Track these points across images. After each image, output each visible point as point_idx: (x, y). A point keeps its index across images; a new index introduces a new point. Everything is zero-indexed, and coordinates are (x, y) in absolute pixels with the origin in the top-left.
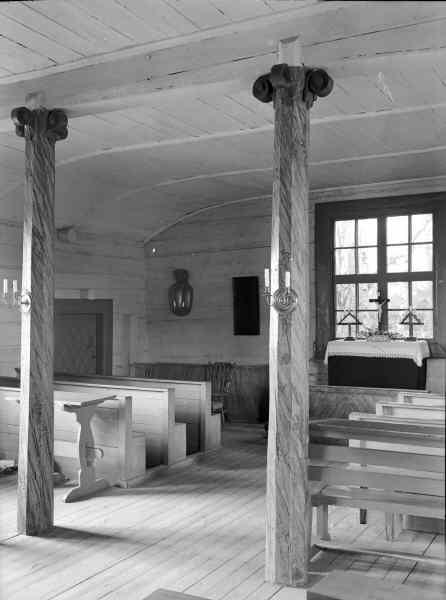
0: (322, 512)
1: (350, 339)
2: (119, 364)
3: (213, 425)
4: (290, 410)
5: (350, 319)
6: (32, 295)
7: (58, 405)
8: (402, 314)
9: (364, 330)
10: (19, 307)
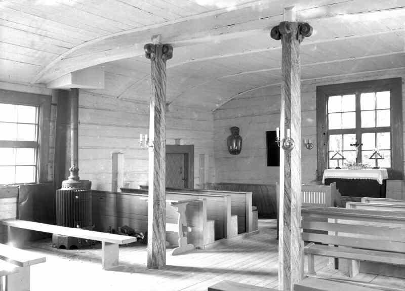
0: (310, 260)
1: (338, 168)
2: (198, 183)
3: (251, 215)
4: (290, 201)
5: (338, 156)
6: (155, 142)
7: (169, 202)
8: (370, 154)
9: (347, 163)
10: (148, 149)
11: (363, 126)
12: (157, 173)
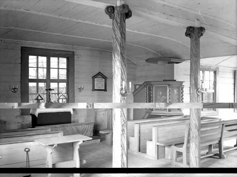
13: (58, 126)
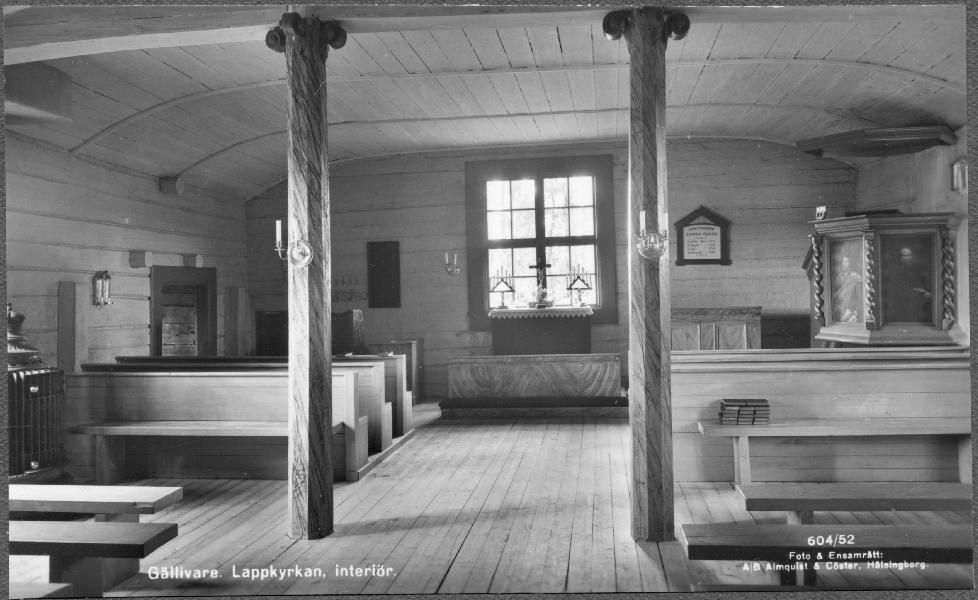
11: (532, 235)
12: (317, 315)
13: (509, 360)
